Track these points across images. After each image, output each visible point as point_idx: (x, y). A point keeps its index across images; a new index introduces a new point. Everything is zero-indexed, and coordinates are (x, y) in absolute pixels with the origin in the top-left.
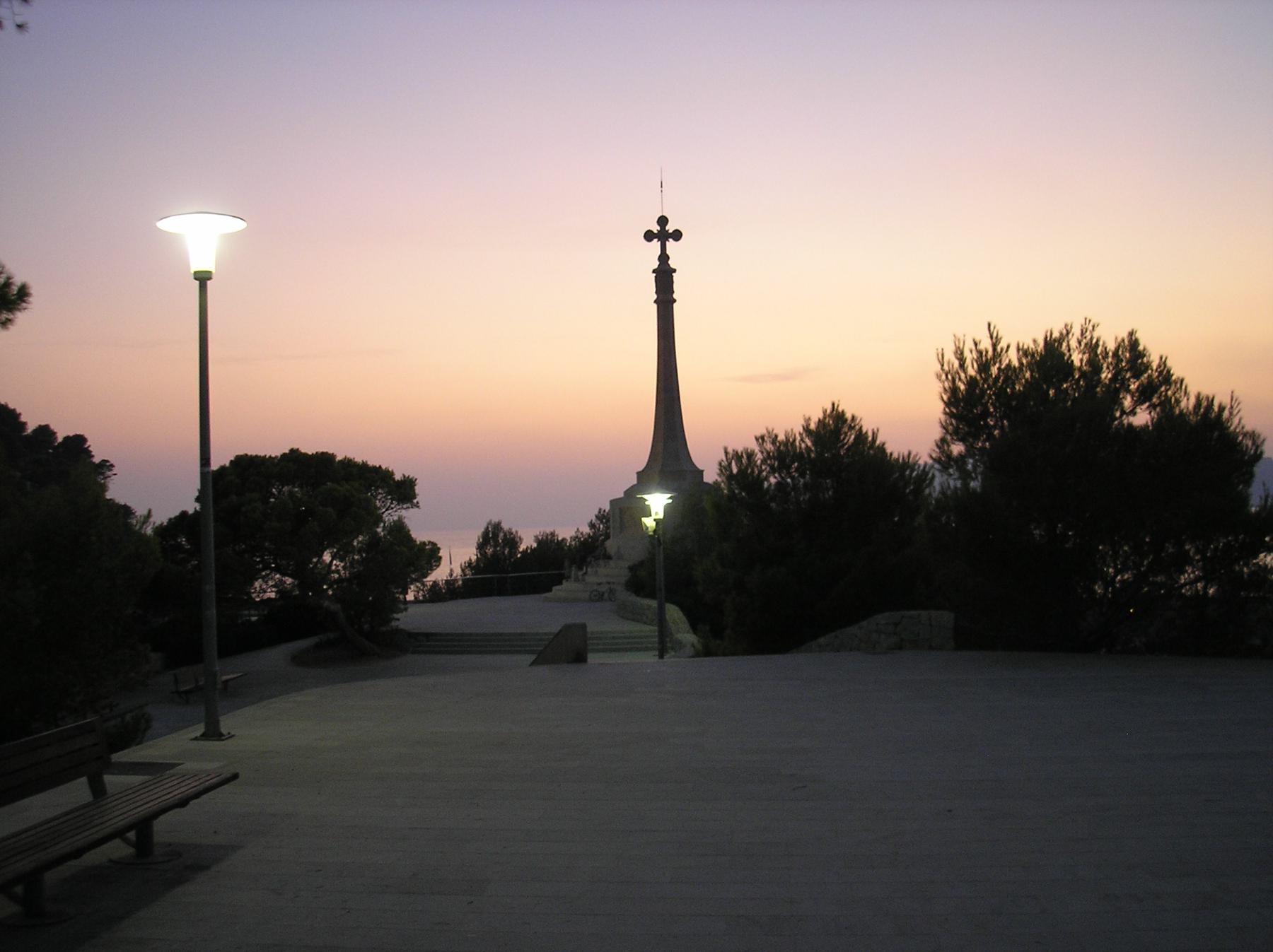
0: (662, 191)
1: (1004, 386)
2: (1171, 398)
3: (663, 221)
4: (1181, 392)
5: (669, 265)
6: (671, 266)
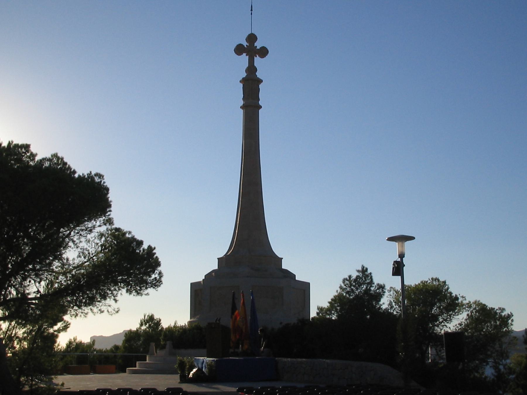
0: (251, 14)
2: (98, 178)
3: (252, 38)
4: (394, 301)
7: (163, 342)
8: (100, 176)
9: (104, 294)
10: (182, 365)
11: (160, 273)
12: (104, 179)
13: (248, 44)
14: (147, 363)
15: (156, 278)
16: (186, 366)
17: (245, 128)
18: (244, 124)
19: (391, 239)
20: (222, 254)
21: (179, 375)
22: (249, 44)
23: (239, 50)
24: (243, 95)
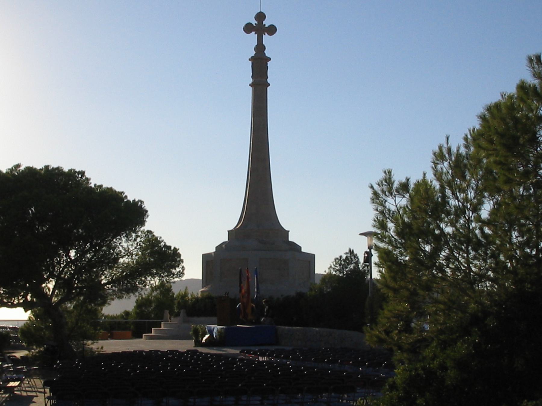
1: (445, 239)
3: (261, 16)
5: (265, 54)
6: (267, 55)
7: (177, 310)
8: (142, 202)
9: (109, 253)
10: (196, 332)
11: (183, 267)
12: (144, 204)
13: (257, 23)
14: (162, 329)
15: (180, 271)
16: (199, 332)
17: (254, 109)
18: (253, 102)
19: (361, 234)
20: (232, 227)
21: (194, 340)
22: (258, 23)
23: (248, 28)
24: (251, 74)
